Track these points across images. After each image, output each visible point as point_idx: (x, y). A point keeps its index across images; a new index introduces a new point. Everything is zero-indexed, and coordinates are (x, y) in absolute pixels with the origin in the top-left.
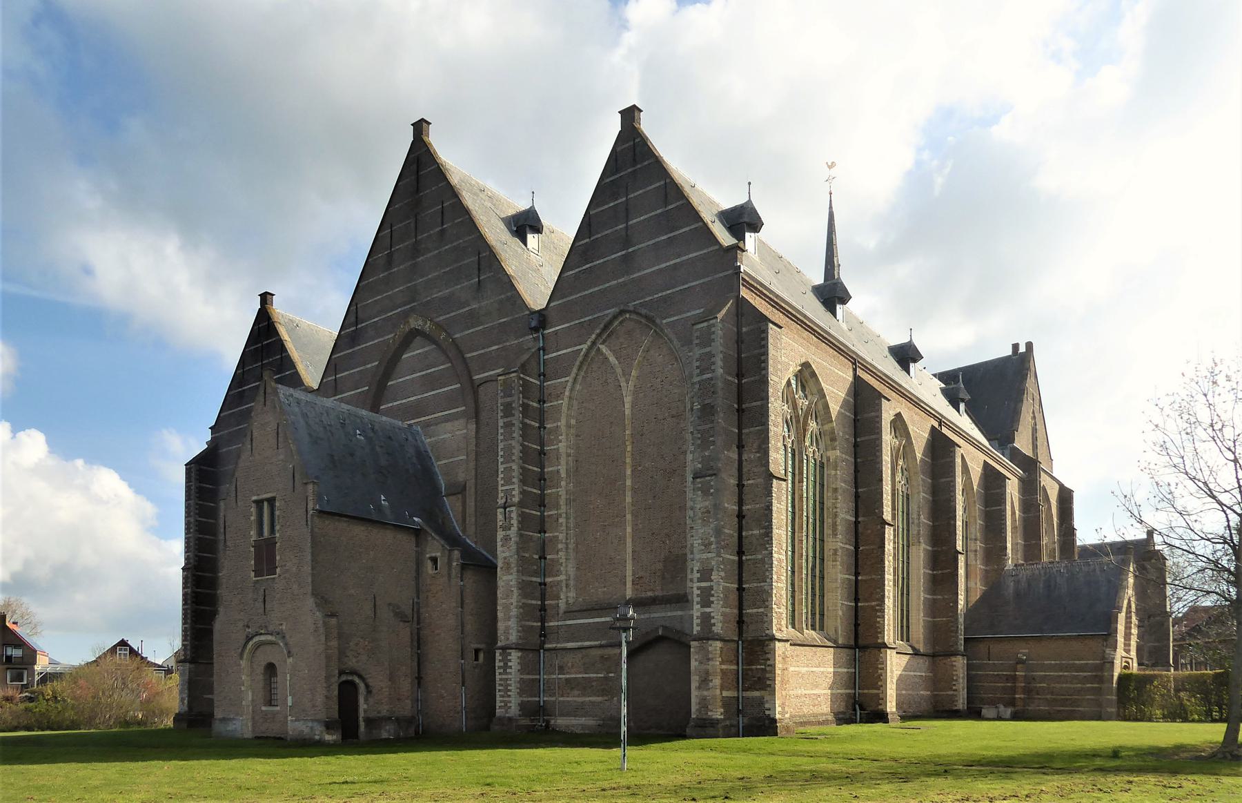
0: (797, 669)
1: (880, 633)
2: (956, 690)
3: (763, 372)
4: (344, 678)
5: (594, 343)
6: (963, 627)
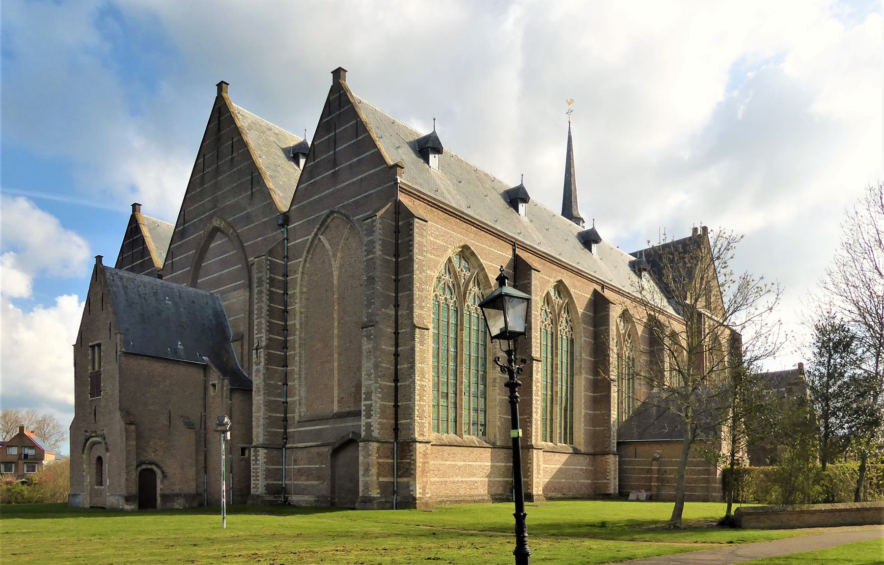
0: (453, 463)
1: (529, 438)
2: (608, 479)
3: (411, 253)
4: (144, 467)
5: (316, 234)
6: (615, 434)
